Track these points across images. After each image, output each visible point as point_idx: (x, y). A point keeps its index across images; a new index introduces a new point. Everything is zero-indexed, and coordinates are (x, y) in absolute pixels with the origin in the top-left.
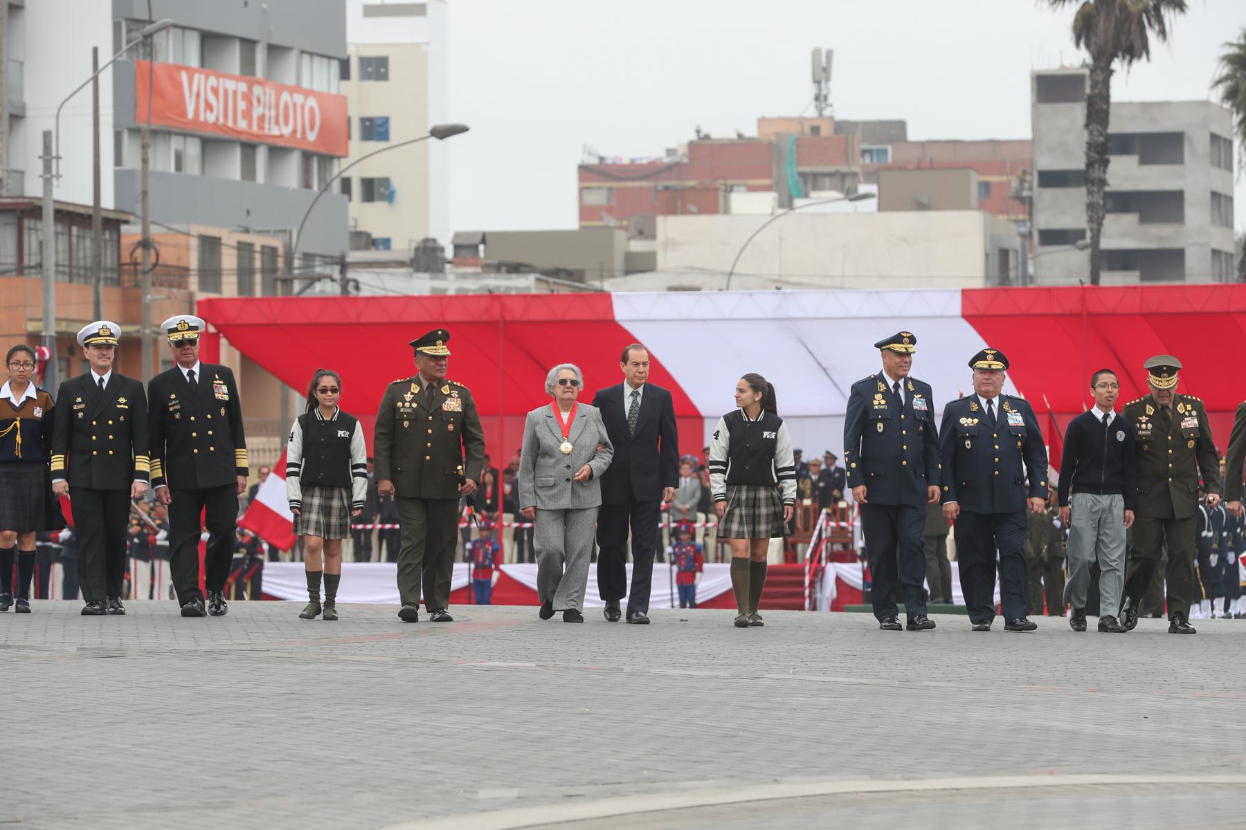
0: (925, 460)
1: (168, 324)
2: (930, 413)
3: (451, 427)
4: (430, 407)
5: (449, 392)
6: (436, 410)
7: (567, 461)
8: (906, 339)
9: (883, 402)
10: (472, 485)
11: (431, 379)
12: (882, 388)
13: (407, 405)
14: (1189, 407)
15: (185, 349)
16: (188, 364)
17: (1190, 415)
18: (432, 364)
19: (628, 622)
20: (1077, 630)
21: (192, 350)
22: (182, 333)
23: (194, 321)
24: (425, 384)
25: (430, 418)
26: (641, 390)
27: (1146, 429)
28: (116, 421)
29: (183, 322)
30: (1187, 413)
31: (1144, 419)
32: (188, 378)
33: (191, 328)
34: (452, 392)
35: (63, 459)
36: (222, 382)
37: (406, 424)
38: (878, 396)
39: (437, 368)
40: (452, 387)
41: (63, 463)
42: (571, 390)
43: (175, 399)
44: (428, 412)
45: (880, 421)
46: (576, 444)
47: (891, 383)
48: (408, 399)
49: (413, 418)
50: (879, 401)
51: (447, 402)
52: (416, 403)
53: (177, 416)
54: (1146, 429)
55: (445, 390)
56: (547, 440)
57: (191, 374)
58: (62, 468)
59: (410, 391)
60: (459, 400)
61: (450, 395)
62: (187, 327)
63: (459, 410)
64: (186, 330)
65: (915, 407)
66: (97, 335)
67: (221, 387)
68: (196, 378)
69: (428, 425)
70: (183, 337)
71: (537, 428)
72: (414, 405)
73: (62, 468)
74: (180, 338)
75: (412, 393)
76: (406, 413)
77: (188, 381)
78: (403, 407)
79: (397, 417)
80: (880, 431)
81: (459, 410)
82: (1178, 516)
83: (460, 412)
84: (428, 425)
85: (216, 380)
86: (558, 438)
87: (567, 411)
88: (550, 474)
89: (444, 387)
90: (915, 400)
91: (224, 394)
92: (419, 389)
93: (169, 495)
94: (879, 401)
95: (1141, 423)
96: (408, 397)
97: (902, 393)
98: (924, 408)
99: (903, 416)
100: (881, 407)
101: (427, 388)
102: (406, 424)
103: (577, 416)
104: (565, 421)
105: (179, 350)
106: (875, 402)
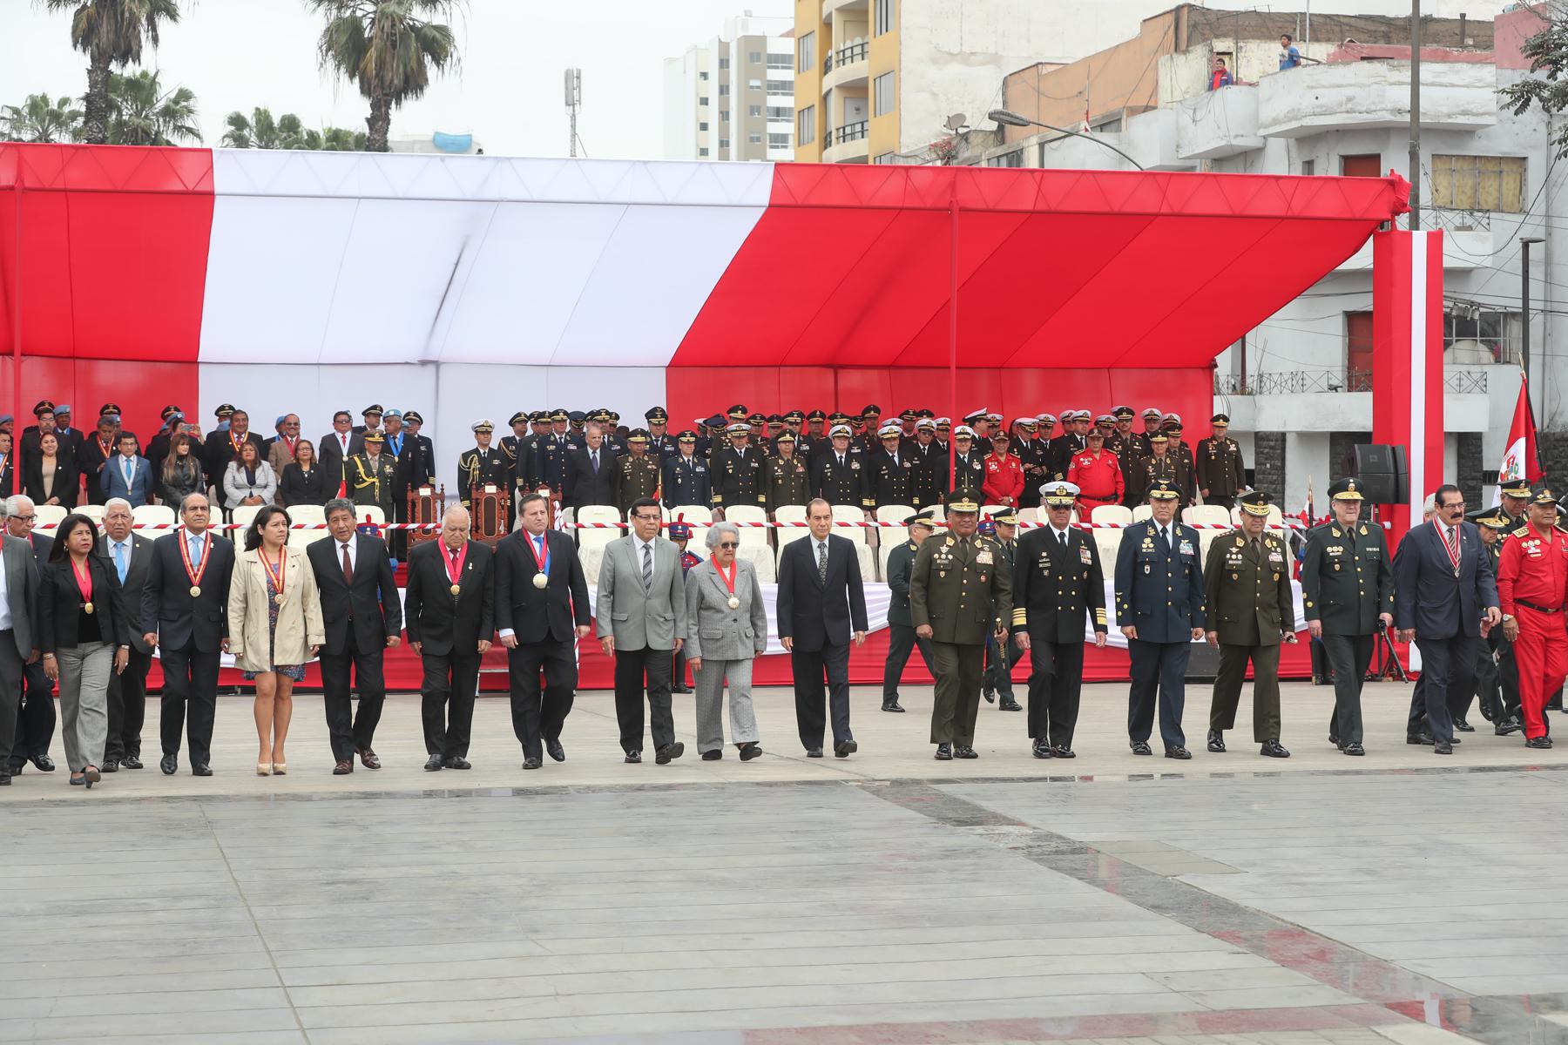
0: (1191, 599)
2: (1196, 557)
3: (983, 578)
4: (1258, 561)
6: (971, 562)
7: (733, 615)
8: (1164, 486)
9: (1151, 545)
10: (1387, 622)
11: (964, 536)
12: (1151, 532)
13: (943, 556)
14: (1275, 544)
16: (1061, 526)
17: (1276, 551)
18: (958, 519)
19: (1167, 756)
20: (1136, 752)
22: (1060, 498)
24: (959, 539)
25: (966, 569)
26: (827, 542)
27: (1237, 559)
28: (1080, 577)
30: (1273, 549)
31: (1234, 550)
33: (1069, 494)
37: (942, 574)
38: (1147, 540)
40: (984, 542)
43: (1046, 557)
45: (1148, 563)
47: (1159, 527)
50: (1147, 545)
51: (980, 555)
53: (1046, 573)
54: (1237, 559)
55: (978, 544)
56: (713, 596)
58: (1025, 623)
60: (991, 554)
61: (982, 549)
62: (1064, 494)
65: (1181, 552)
66: (839, 431)
68: (1066, 540)
72: (950, 557)
73: (1025, 623)
74: (1058, 502)
75: (947, 546)
78: (940, 558)
79: (934, 567)
80: (1147, 573)
87: (726, 567)
88: (718, 627)
90: (1182, 545)
92: (953, 542)
94: (1147, 545)
95: (1231, 553)
96: (944, 549)
97: (1170, 538)
98: (1191, 552)
99: (1169, 560)
100: (1149, 550)
102: (942, 574)
103: (738, 571)
104: (728, 576)
105: (1055, 513)
106: (1144, 546)
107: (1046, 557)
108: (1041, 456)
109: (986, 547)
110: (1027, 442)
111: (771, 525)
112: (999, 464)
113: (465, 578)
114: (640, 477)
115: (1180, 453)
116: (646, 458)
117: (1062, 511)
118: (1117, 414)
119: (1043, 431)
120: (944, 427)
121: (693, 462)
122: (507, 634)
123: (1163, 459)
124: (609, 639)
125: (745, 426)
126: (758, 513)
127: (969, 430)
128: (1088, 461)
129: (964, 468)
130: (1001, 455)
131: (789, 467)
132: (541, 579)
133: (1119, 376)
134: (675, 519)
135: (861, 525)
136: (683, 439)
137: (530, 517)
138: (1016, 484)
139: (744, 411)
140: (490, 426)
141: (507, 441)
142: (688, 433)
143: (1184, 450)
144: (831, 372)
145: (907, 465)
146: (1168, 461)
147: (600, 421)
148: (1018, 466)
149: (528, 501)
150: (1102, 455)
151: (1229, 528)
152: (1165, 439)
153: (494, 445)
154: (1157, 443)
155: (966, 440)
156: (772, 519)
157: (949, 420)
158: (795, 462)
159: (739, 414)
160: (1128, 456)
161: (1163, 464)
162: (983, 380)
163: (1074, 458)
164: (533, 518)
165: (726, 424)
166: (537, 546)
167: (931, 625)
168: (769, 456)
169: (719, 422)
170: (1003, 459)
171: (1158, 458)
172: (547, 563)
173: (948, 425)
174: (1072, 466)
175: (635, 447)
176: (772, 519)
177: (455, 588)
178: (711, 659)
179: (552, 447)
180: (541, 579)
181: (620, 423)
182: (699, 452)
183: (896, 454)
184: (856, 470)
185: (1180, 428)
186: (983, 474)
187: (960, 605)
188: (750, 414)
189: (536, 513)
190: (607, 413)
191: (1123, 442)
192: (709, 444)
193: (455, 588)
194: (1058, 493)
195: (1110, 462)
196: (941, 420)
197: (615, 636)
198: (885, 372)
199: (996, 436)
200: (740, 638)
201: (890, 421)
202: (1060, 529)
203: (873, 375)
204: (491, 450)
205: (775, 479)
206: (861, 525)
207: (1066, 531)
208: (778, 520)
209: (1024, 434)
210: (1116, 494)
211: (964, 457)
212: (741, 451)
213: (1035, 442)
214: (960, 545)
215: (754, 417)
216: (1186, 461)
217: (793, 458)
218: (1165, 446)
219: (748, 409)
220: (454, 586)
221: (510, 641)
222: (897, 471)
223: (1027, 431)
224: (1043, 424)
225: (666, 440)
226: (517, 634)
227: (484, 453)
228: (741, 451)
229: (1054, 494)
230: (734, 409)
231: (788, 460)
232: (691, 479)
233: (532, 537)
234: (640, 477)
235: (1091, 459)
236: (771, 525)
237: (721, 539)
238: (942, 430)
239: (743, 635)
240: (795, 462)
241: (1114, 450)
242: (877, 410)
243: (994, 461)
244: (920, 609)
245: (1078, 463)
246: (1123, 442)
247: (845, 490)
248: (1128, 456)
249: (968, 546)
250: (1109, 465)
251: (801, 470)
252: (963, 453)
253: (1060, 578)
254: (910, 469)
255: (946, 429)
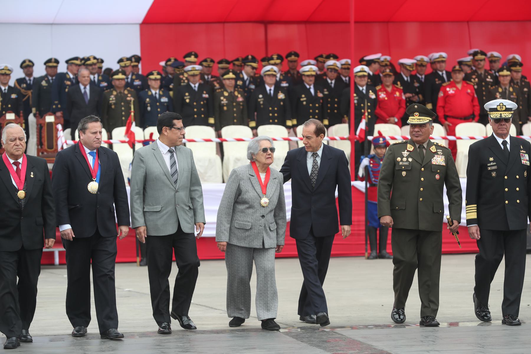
1: (491, 104)
3: (437, 177)
4: (422, 163)
5: (436, 151)
13: (405, 159)
15: (501, 125)
16: (503, 136)
21: (506, 126)
22: (502, 113)
23: (509, 104)
28: (521, 175)
29: (501, 104)
32: (502, 147)
33: (507, 110)
34: (438, 150)
35: (476, 210)
36: (525, 152)
39: (500, 127)
41: (476, 213)
42: (270, 156)
43: (493, 162)
44: (421, 165)
46: (271, 200)
48: (405, 156)
49: (410, 169)
51: (435, 158)
52: (412, 157)
53: (494, 174)
57: (505, 143)
59: (407, 149)
60: (443, 157)
61: (436, 153)
62: (504, 108)
63: (443, 164)
64: (504, 111)
66: (269, 71)
67: (524, 155)
68: (508, 146)
69: (420, 174)
70: (501, 116)
71: (242, 183)
72: (410, 160)
74: (498, 117)
75: (408, 151)
76: (404, 166)
77: (503, 148)
78: (402, 161)
79: (397, 168)
81: (443, 164)
82: (266, 246)
83: (444, 166)
84: (420, 174)
85: (522, 150)
86: (259, 193)
89: (432, 148)
91: (527, 161)
92: (413, 148)
93: (479, 232)
101: (419, 147)
102: (404, 173)
104: (263, 180)
105: (497, 125)
107: (493, 162)
108: (418, 87)
109: (440, 151)
110: (407, 77)
111: (218, 140)
112: (387, 94)
113: (28, 184)
114: (122, 106)
115: (521, 83)
116: (126, 92)
117: (503, 123)
118: (475, 54)
119: (419, 68)
120: (346, 66)
121: (160, 95)
122: (67, 227)
123: (507, 88)
124: (142, 229)
125: (198, 67)
126: (209, 132)
127: (366, 68)
128: (453, 90)
129: (363, 97)
130: (388, 86)
131: (232, 98)
132: (93, 186)
133: (476, 28)
134: (147, 138)
135: (285, 139)
136: (152, 77)
137: (91, 135)
138: (400, 108)
139: (196, 56)
140: (9, 70)
141: (20, 81)
142: (275, 57)
143: (524, 81)
144: (261, 29)
145: (320, 95)
146: (511, 89)
147: (91, 65)
148: (400, 94)
149: (91, 122)
150: (463, 87)
151: (400, 140)
152: (509, 73)
153: (12, 83)
154: (503, 76)
155: (364, 76)
156: (219, 136)
157: (349, 61)
158: (236, 93)
159: (192, 59)
160: (482, 86)
161: (507, 92)
162: (377, 30)
163: (442, 88)
164: (93, 136)
165: (184, 66)
166: (91, 160)
167: (393, 216)
168: (219, 89)
169: (180, 65)
170: (389, 89)
171: (503, 87)
172: (98, 173)
173: (349, 65)
174: (441, 94)
175: (117, 83)
176: (219, 136)
177: (21, 194)
178: (239, 245)
179: (69, 83)
180: (93, 186)
181: (105, 66)
182: (164, 86)
183: (312, 87)
184: (281, 100)
185: (521, 65)
186: (377, 102)
187: (418, 199)
188: (202, 58)
189: (96, 133)
190: (95, 58)
191: (479, 76)
192: (171, 81)
193: (21, 194)
194: (499, 109)
195: (469, 91)
196: (343, 61)
197: (146, 226)
198: (302, 27)
199: (384, 72)
200: (266, 230)
201: (306, 62)
202: (502, 138)
203: (294, 29)
204: (10, 87)
205: (221, 106)
206: (285, 139)
207: (508, 139)
208: (224, 137)
209: (405, 71)
210: (473, 114)
211: (363, 89)
212: (195, 86)
213: (413, 77)
214: (418, 150)
215: (205, 61)
216: (526, 90)
217: (235, 90)
218: (509, 78)
219: (199, 55)
220: (20, 192)
221: (68, 234)
222: (312, 99)
223: (407, 70)
224: (419, 63)
225: (134, 77)
226: (73, 229)
227: (5, 90)
228: (195, 86)
229: (495, 110)
230: (189, 55)
231: (231, 92)
232: (157, 107)
233: (87, 151)
234: (122, 106)
235: (455, 89)
236: (218, 140)
237: (261, 146)
238: (345, 69)
239: (268, 229)
240: (236, 93)
241: (471, 82)
242: (297, 55)
243: (383, 91)
244: (386, 205)
245: (445, 92)
246: (479, 76)
247: (273, 114)
248: (482, 86)
249: (424, 151)
250: (468, 93)
251: (240, 99)
252: (362, 86)
253: (506, 177)
254: (322, 98)
255: (348, 68)
